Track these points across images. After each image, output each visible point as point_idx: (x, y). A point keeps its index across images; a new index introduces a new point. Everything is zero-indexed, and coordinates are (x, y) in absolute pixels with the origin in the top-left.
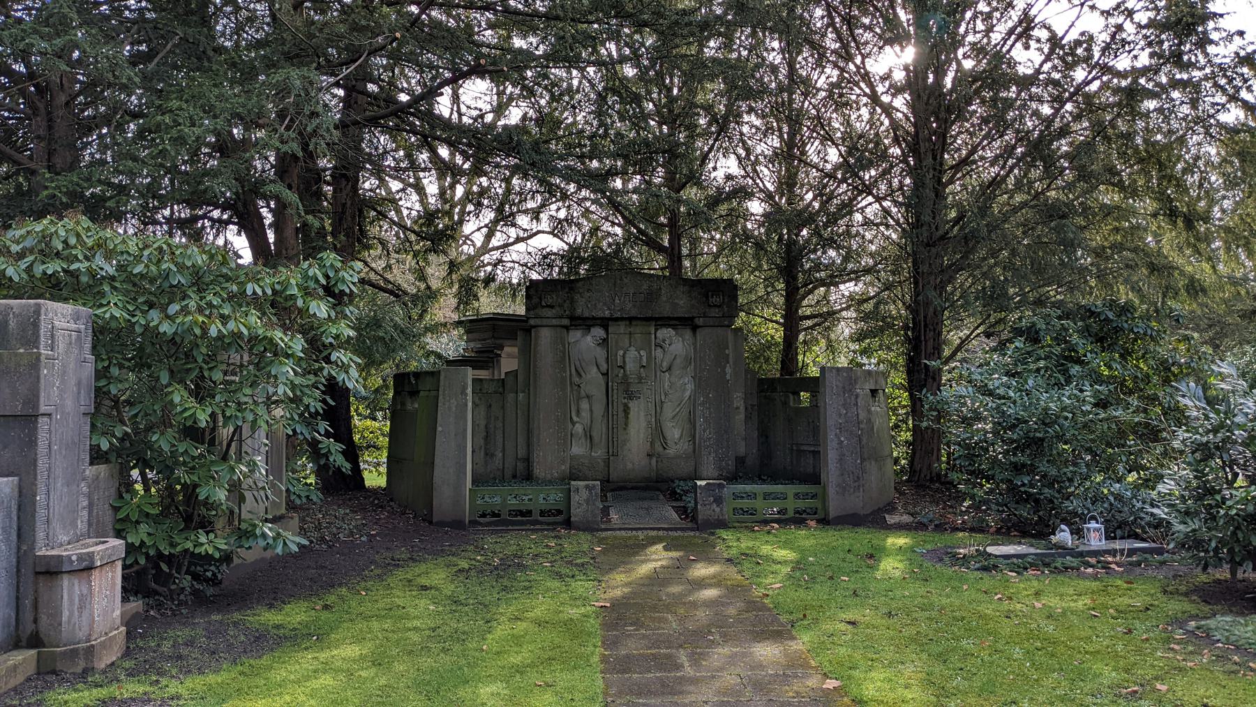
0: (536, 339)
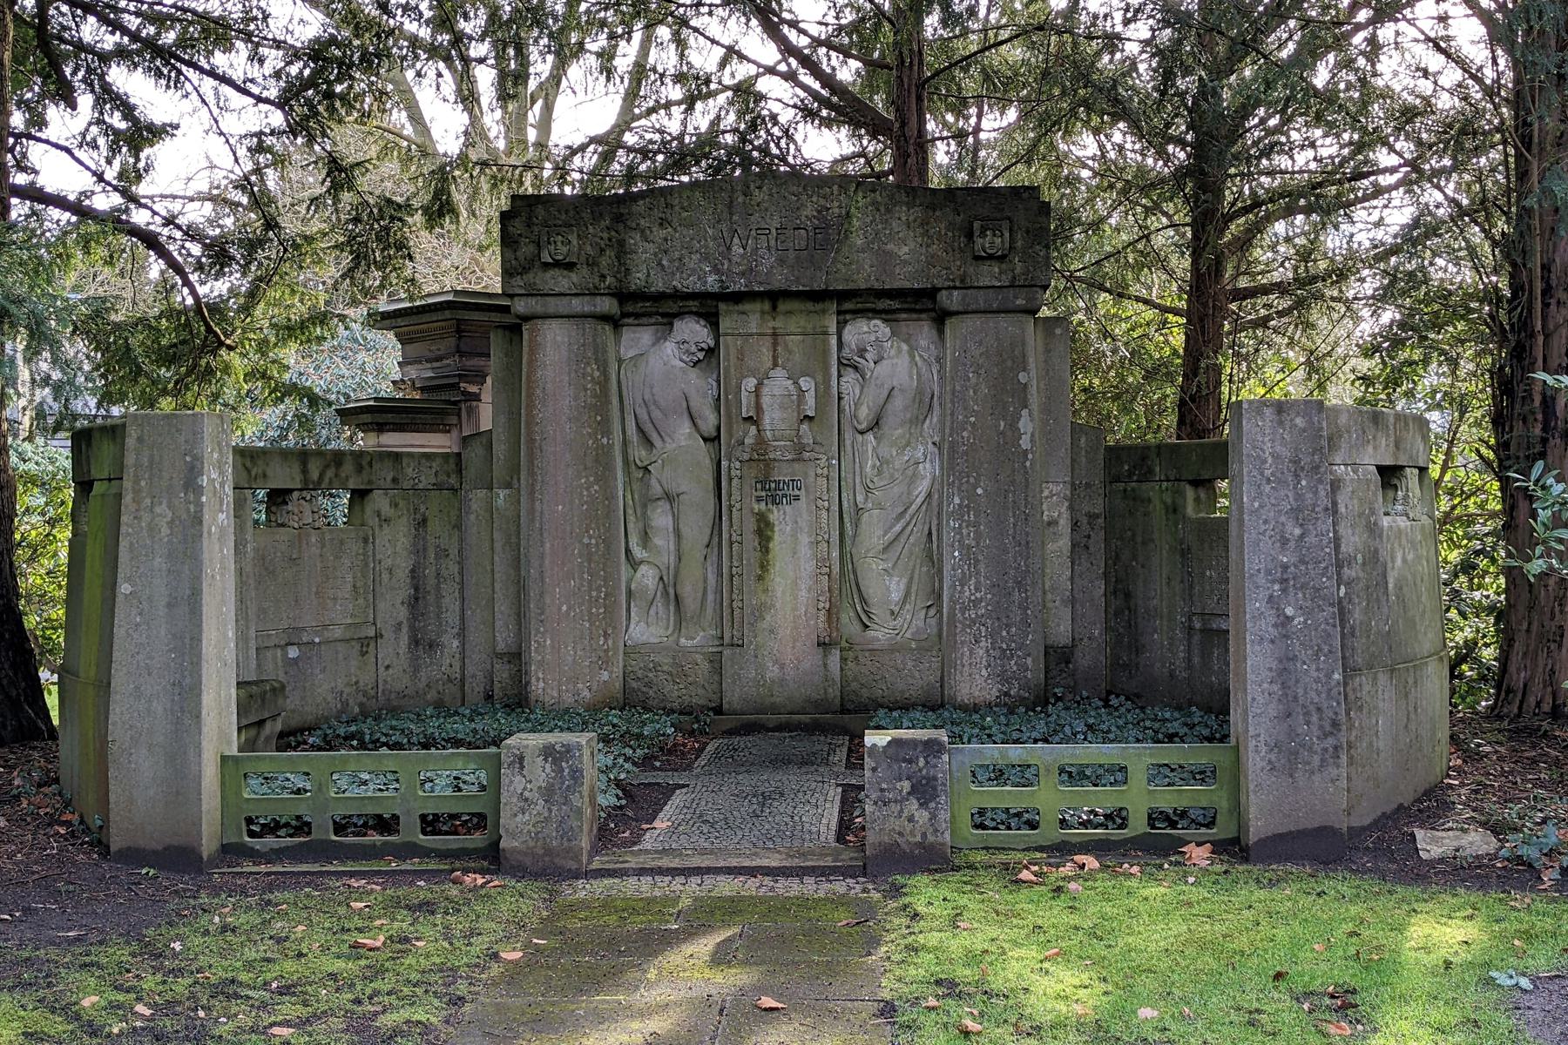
0: (532, 352)
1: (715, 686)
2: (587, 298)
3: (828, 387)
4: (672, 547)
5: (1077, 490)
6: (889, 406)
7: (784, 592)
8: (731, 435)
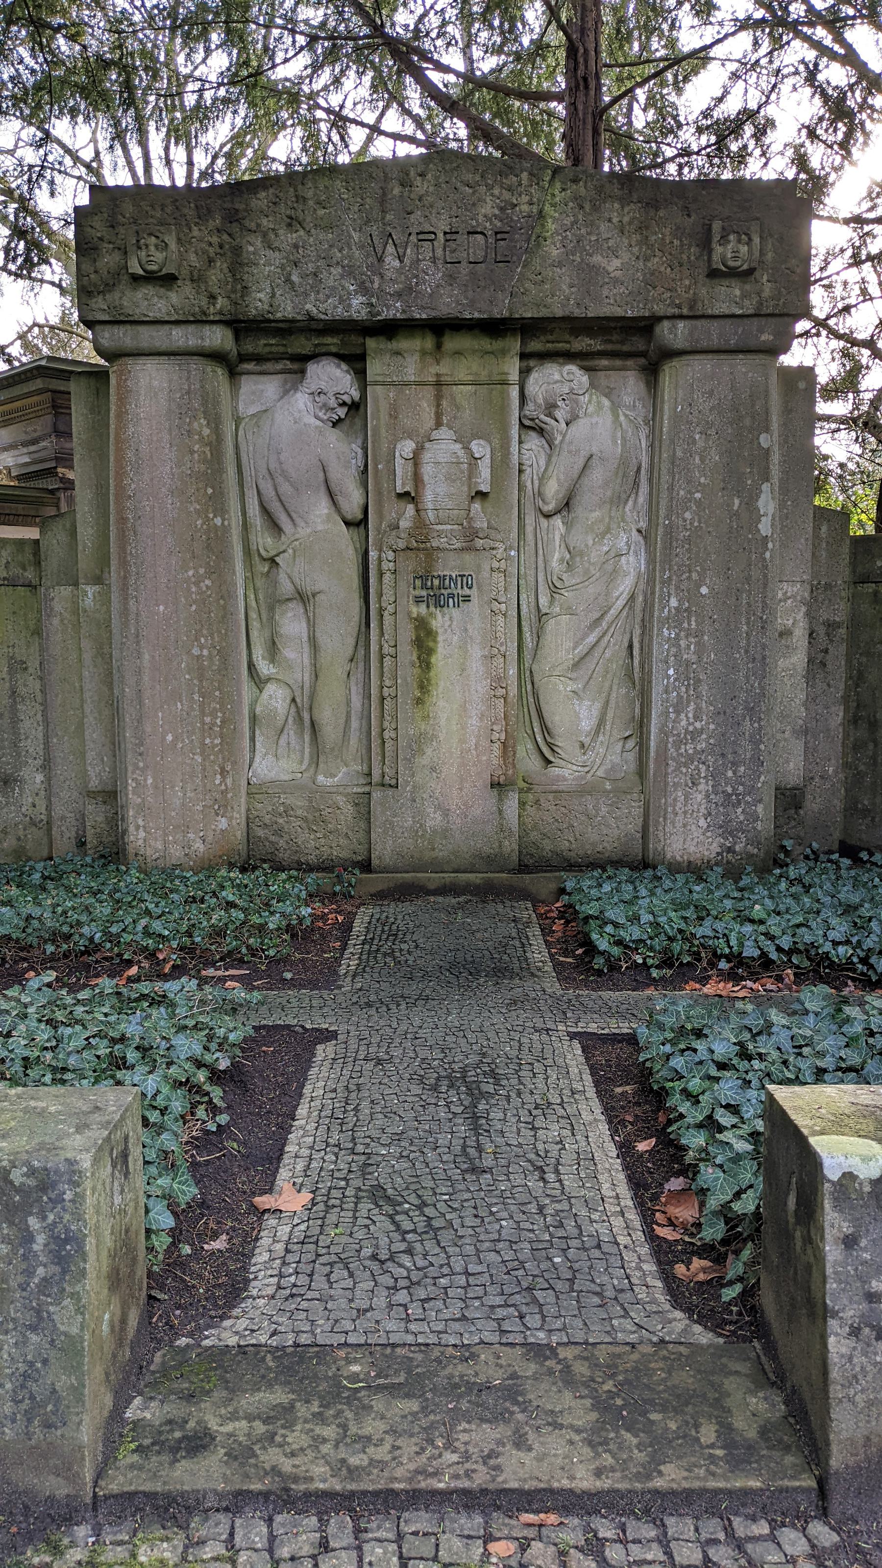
0: (122, 401)
1: (361, 835)
2: (191, 328)
3: (506, 454)
4: (306, 661)
5: (819, 592)
6: (585, 481)
7: (448, 719)
8: (380, 516)
